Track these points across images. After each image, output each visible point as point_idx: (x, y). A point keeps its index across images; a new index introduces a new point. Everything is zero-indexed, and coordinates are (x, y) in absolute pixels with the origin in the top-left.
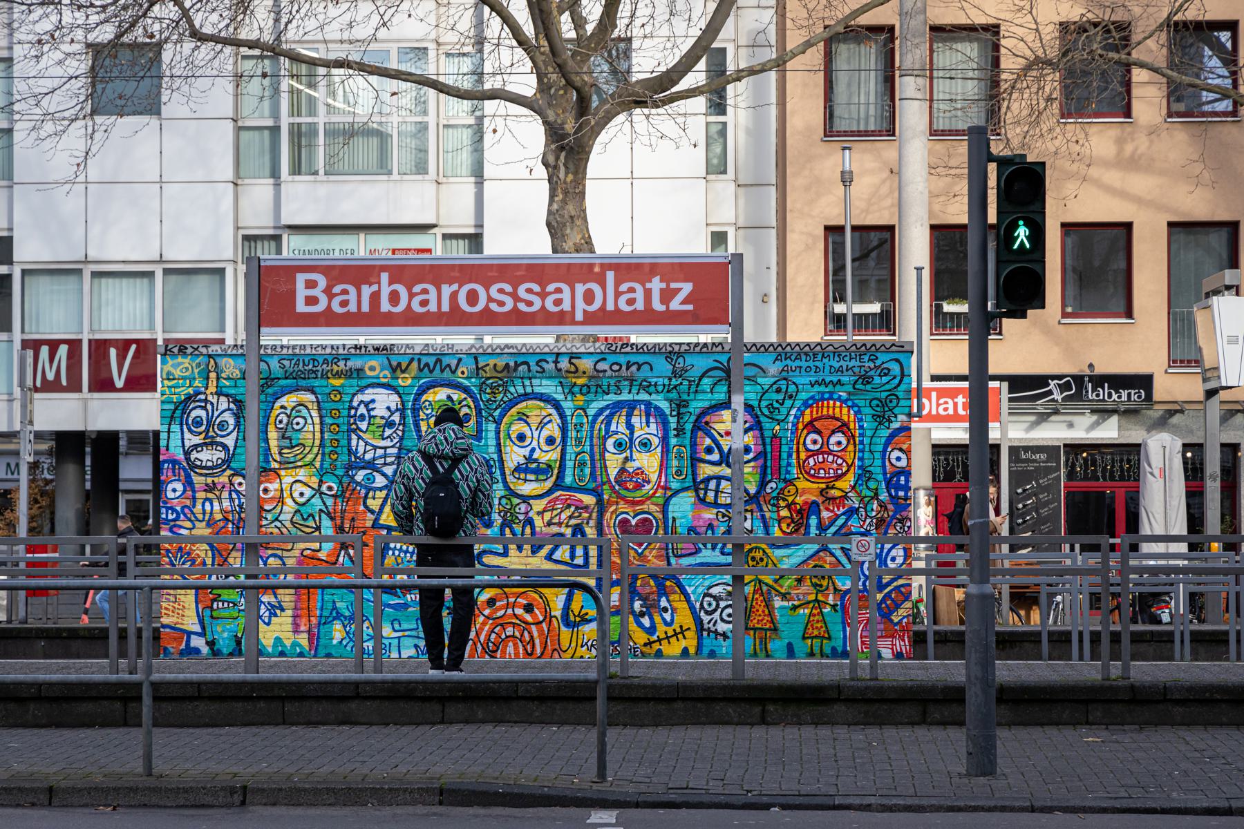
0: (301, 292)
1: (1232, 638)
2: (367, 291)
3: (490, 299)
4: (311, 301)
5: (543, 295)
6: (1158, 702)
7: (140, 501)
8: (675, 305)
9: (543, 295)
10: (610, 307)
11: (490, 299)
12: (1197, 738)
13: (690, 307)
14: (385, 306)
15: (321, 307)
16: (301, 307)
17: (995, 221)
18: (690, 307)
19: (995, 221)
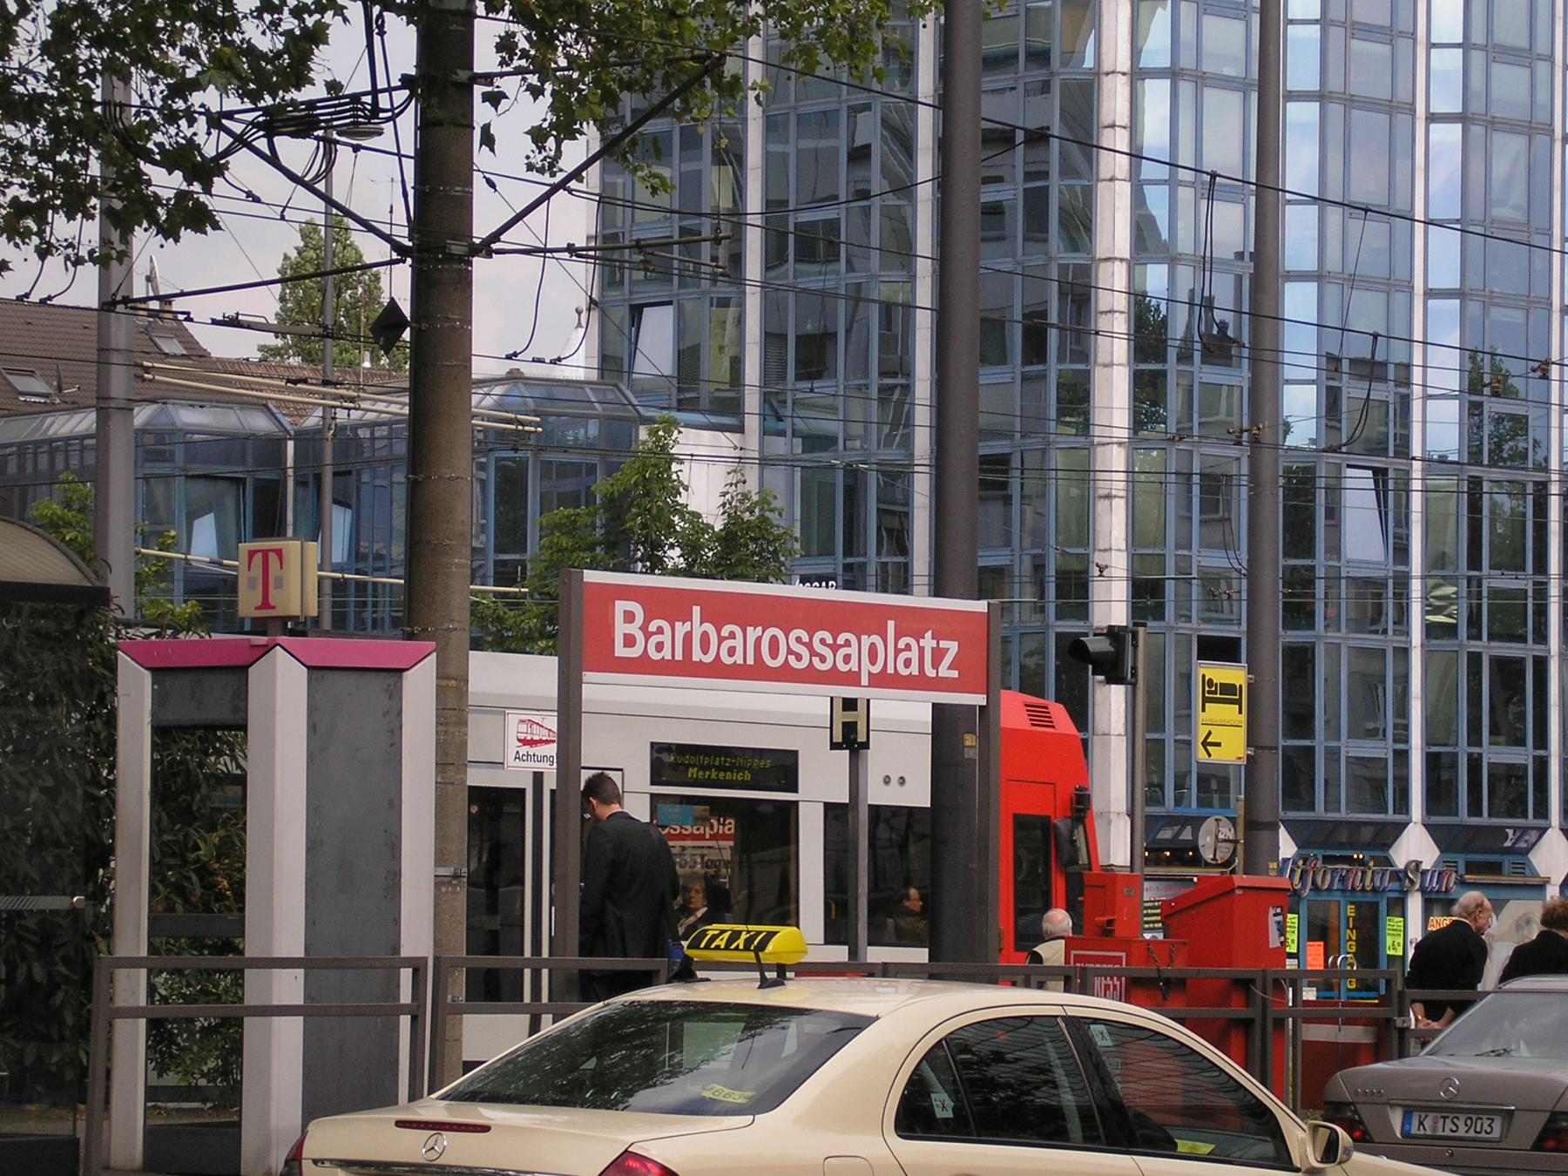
0: (621, 628)
1: (1016, 462)
2: (681, 629)
3: (790, 651)
4: (630, 641)
5: (835, 648)
6: (793, 967)
7: (1296, 557)
8: (945, 671)
9: (835, 648)
10: (930, 672)
11: (790, 651)
12: (1180, 211)
13: (955, 674)
14: (697, 655)
15: (635, 652)
16: (621, 651)
17: (409, 1001)
18: (955, 674)
19: (409, 1001)
